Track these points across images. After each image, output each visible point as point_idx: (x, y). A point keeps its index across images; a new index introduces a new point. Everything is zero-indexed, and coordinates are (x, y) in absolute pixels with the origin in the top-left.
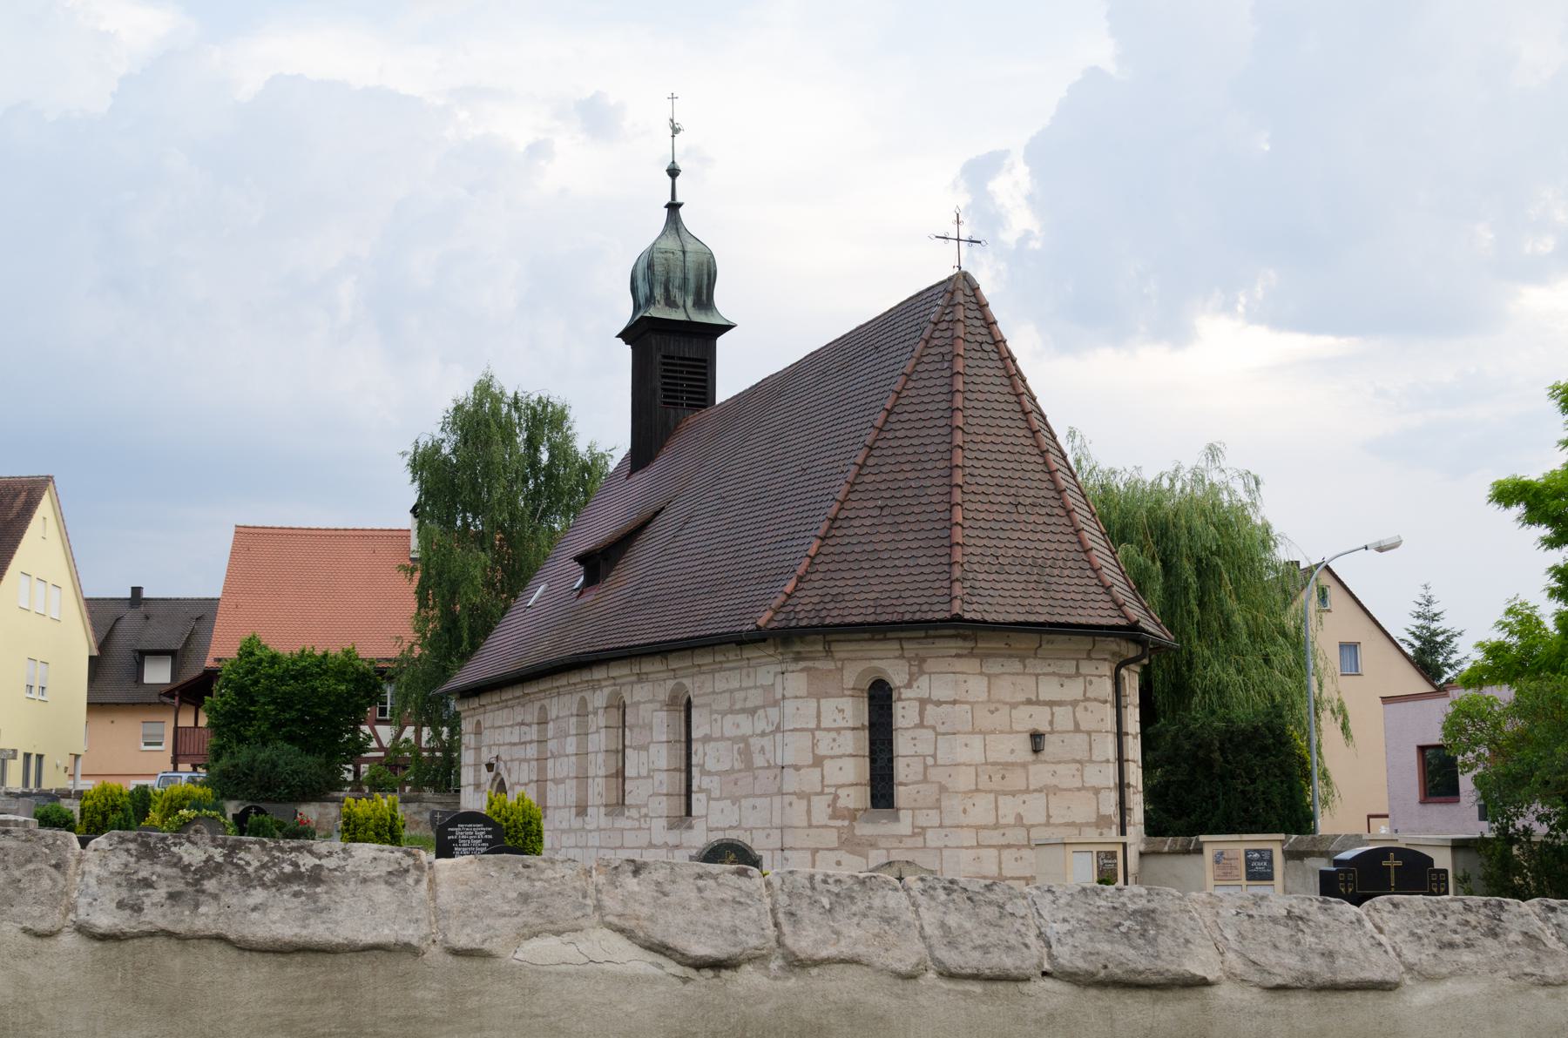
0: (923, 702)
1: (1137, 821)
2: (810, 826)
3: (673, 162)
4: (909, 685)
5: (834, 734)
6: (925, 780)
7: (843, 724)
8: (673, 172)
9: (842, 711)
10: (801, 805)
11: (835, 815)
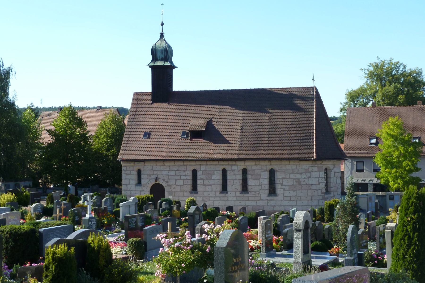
0: (335, 172)
1: (124, 178)
2: (318, 196)
3: (162, 22)
4: (333, 169)
5: (322, 178)
6: (335, 187)
7: (323, 177)
8: (162, 24)
9: (323, 174)
10: (316, 192)
11: (322, 193)
